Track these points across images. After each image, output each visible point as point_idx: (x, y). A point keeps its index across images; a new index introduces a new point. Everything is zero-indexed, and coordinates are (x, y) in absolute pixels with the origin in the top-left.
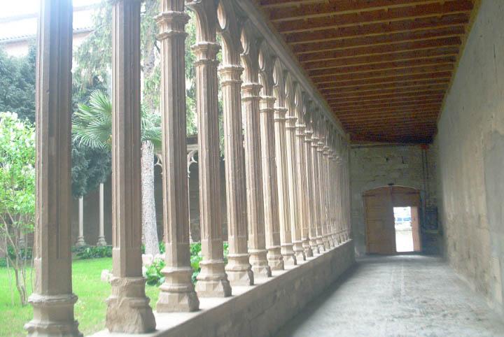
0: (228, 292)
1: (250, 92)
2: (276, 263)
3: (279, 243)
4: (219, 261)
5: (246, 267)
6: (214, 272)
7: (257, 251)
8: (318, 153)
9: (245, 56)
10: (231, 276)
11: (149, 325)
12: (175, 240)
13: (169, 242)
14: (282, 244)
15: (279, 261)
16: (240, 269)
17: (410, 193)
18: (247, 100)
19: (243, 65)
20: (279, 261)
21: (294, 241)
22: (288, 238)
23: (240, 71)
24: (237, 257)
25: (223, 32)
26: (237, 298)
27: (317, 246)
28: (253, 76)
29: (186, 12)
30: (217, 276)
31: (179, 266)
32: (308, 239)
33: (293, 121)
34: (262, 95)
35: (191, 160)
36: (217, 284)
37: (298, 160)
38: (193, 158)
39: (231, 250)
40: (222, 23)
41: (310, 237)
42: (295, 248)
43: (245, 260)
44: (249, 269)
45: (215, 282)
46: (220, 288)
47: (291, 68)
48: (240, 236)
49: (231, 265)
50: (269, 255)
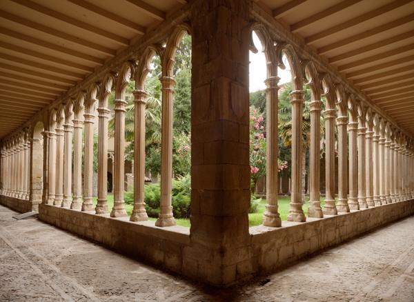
0: (348, 211)
1: (362, 131)
8: (391, 150)
9: (360, 118)
10: (338, 208)
14: (367, 196)
17: (213, 256)
18: (340, 125)
19: (338, 107)
21: (381, 195)
22: (378, 193)
23: (372, 133)
25: (340, 104)
26: (352, 214)
28: (355, 118)
32: (390, 195)
33: (384, 140)
37: (386, 158)
39: (360, 196)
40: (326, 90)
41: (391, 194)
42: (381, 198)
44: (358, 204)
46: (345, 209)
47: (377, 111)
50: (367, 200)
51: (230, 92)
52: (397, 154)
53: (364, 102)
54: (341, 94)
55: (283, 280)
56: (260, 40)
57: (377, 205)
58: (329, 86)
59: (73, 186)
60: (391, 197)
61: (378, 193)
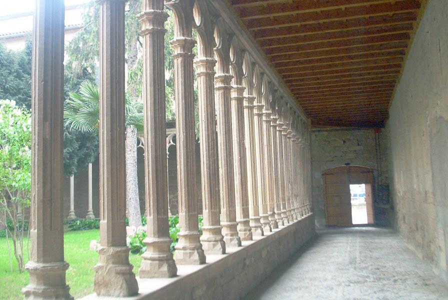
0: (203, 260)
2: (245, 234)
3: (248, 216)
4: (195, 233)
5: (219, 238)
6: (244, 226)
7: (229, 223)
9: (218, 50)
10: (205, 246)
11: (132, 290)
12: (156, 214)
13: (150, 215)
15: (248, 233)
16: (214, 239)
18: (219, 89)
20: (248, 233)
21: (261, 215)
22: (256, 212)
23: (242, 90)
24: (210, 229)
27: (282, 219)
29: (165, 10)
30: (193, 246)
31: (159, 237)
32: (274, 213)
34: (233, 84)
35: (170, 142)
36: (193, 253)
37: (265, 143)
38: (171, 141)
41: (276, 211)
42: (262, 221)
43: (217, 232)
44: (222, 240)
45: (191, 251)
46: (196, 256)
47: (267, 72)
48: (213, 210)
49: (205, 236)
51: (37, 9)
52: (281, 136)
53: (290, 104)
54: (220, 36)
55: (375, 142)
56: (373, 209)
57: (257, 237)
58: (202, 14)
59: (103, 203)
60: (276, 217)
61: (256, 212)
